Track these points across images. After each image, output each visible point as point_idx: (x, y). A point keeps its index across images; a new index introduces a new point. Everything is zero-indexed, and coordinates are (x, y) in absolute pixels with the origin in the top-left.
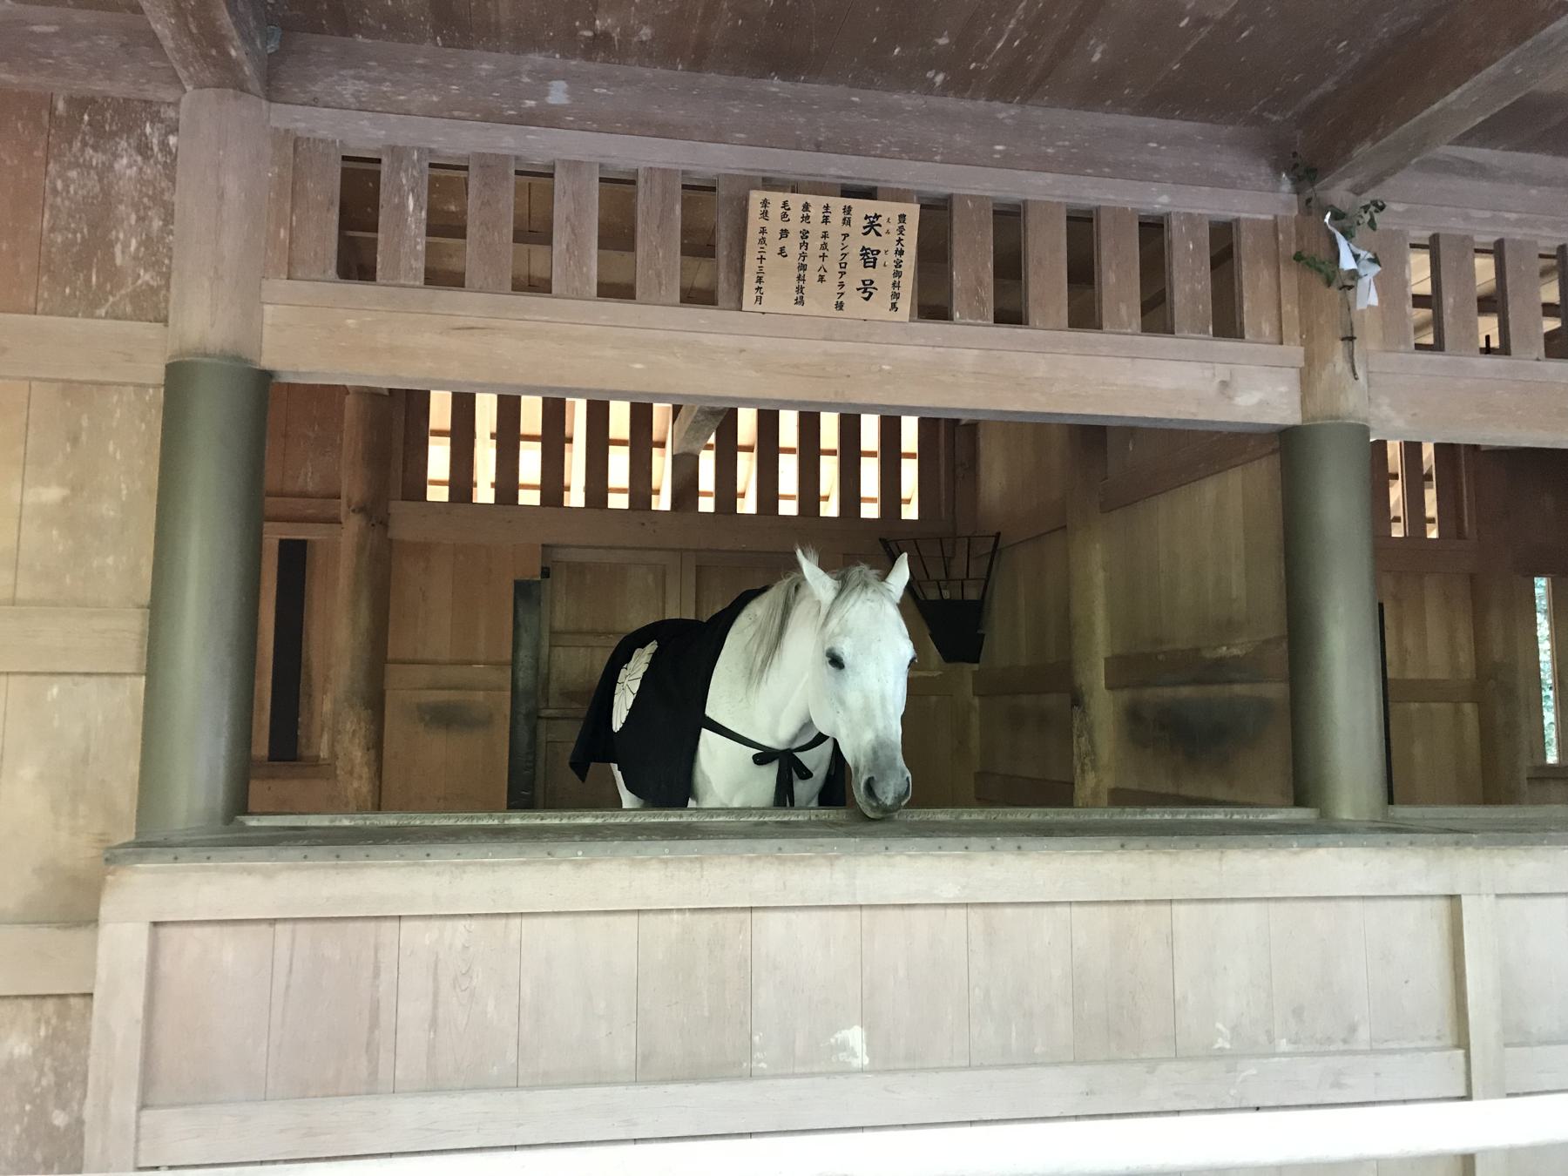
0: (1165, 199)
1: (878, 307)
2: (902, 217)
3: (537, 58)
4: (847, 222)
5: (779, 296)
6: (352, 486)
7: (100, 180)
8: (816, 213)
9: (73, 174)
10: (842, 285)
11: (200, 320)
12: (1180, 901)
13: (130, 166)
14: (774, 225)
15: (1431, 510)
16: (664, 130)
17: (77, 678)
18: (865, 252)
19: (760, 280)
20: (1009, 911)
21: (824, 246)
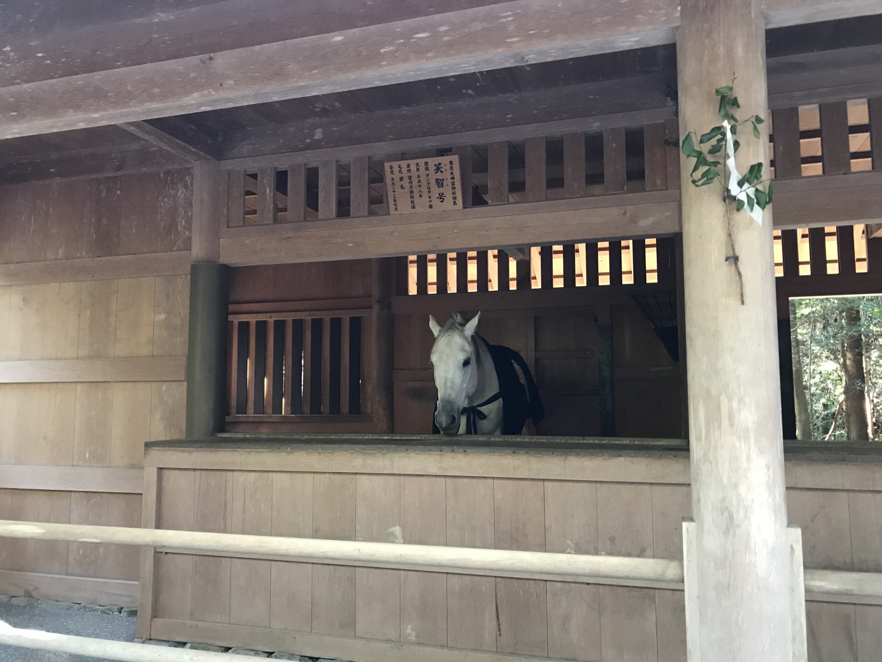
0: (597, 124)
1: (448, 204)
2: (451, 162)
3: (310, 121)
4: (427, 169)
5: (404, 205)
6: (376, 292)
8: (413, 168)
9: (166, 200)
10: (430, 197)
11: (198, 250)
12: (548, 480)
14: (397, 176)
18: (437, 181)
19: (395, 201)
20: (465, 480)
21: (419, 181)
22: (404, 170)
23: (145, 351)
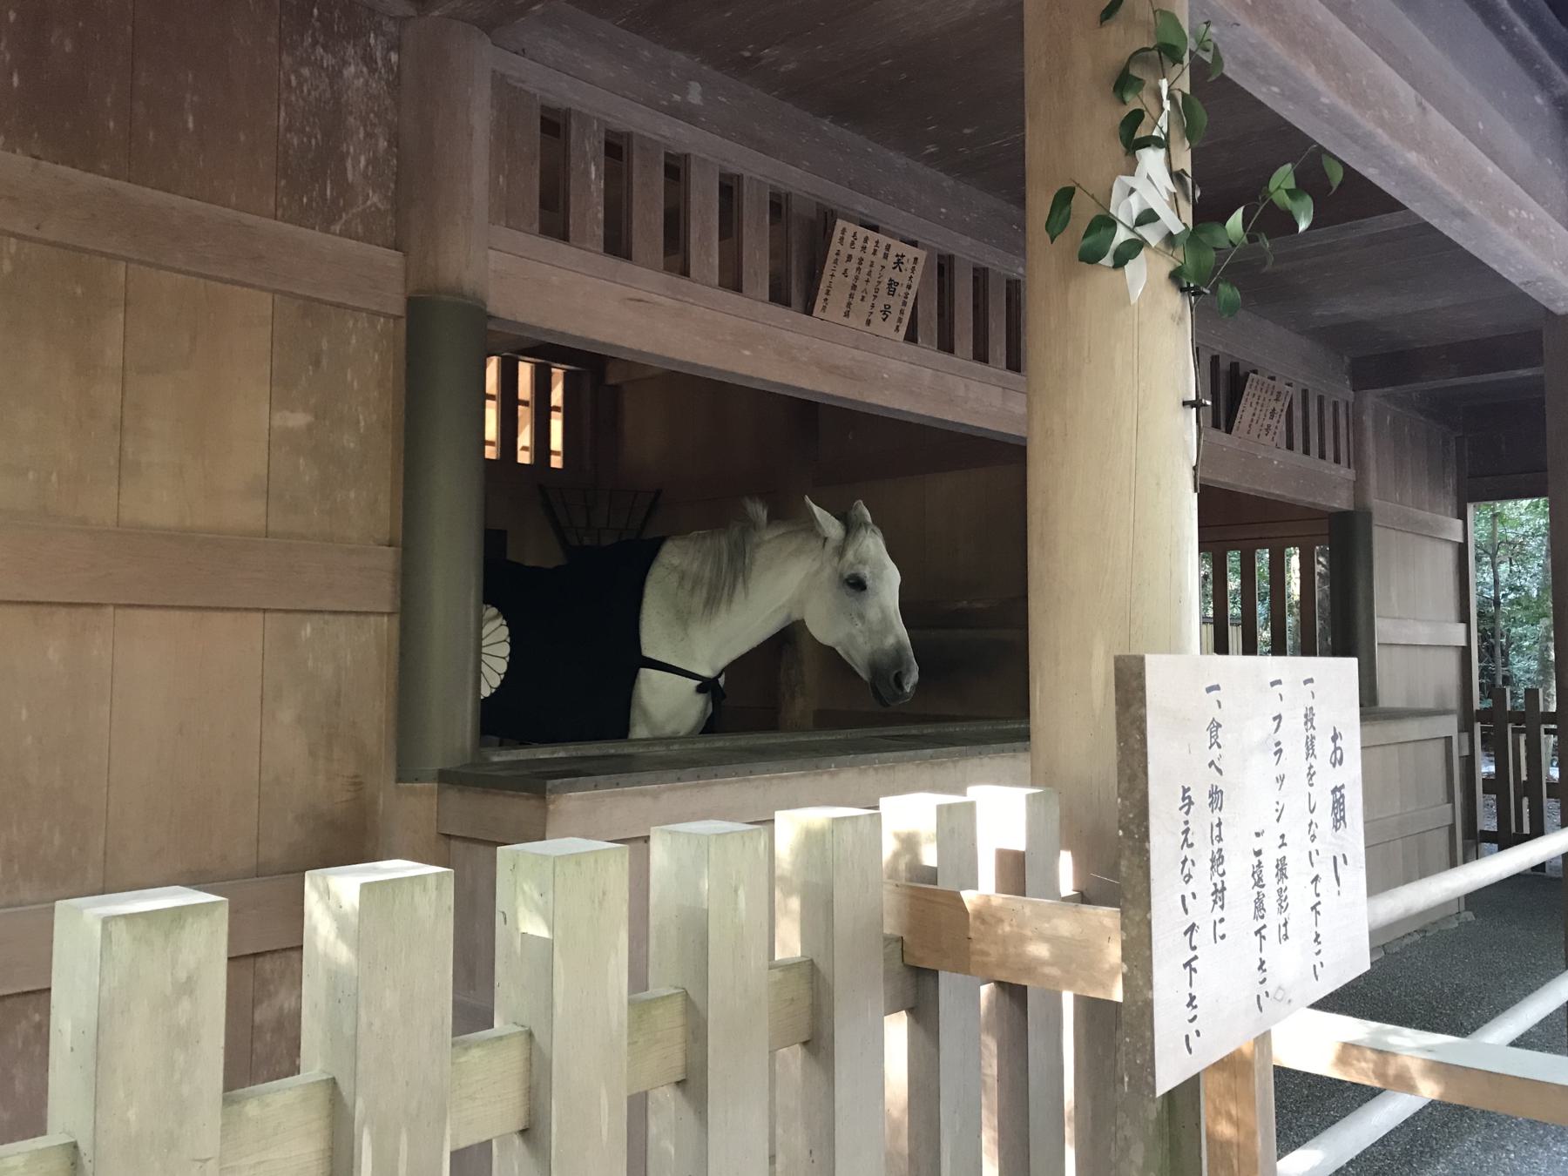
4: (886, 256)
7: (331, 85)
9: (306, 72)
13: (357, 75)
15: (556, 442)
16: (762, 146)
17: (327, 617)
19: (828, 293)
22: (859, 243)
23: (246, 514)
